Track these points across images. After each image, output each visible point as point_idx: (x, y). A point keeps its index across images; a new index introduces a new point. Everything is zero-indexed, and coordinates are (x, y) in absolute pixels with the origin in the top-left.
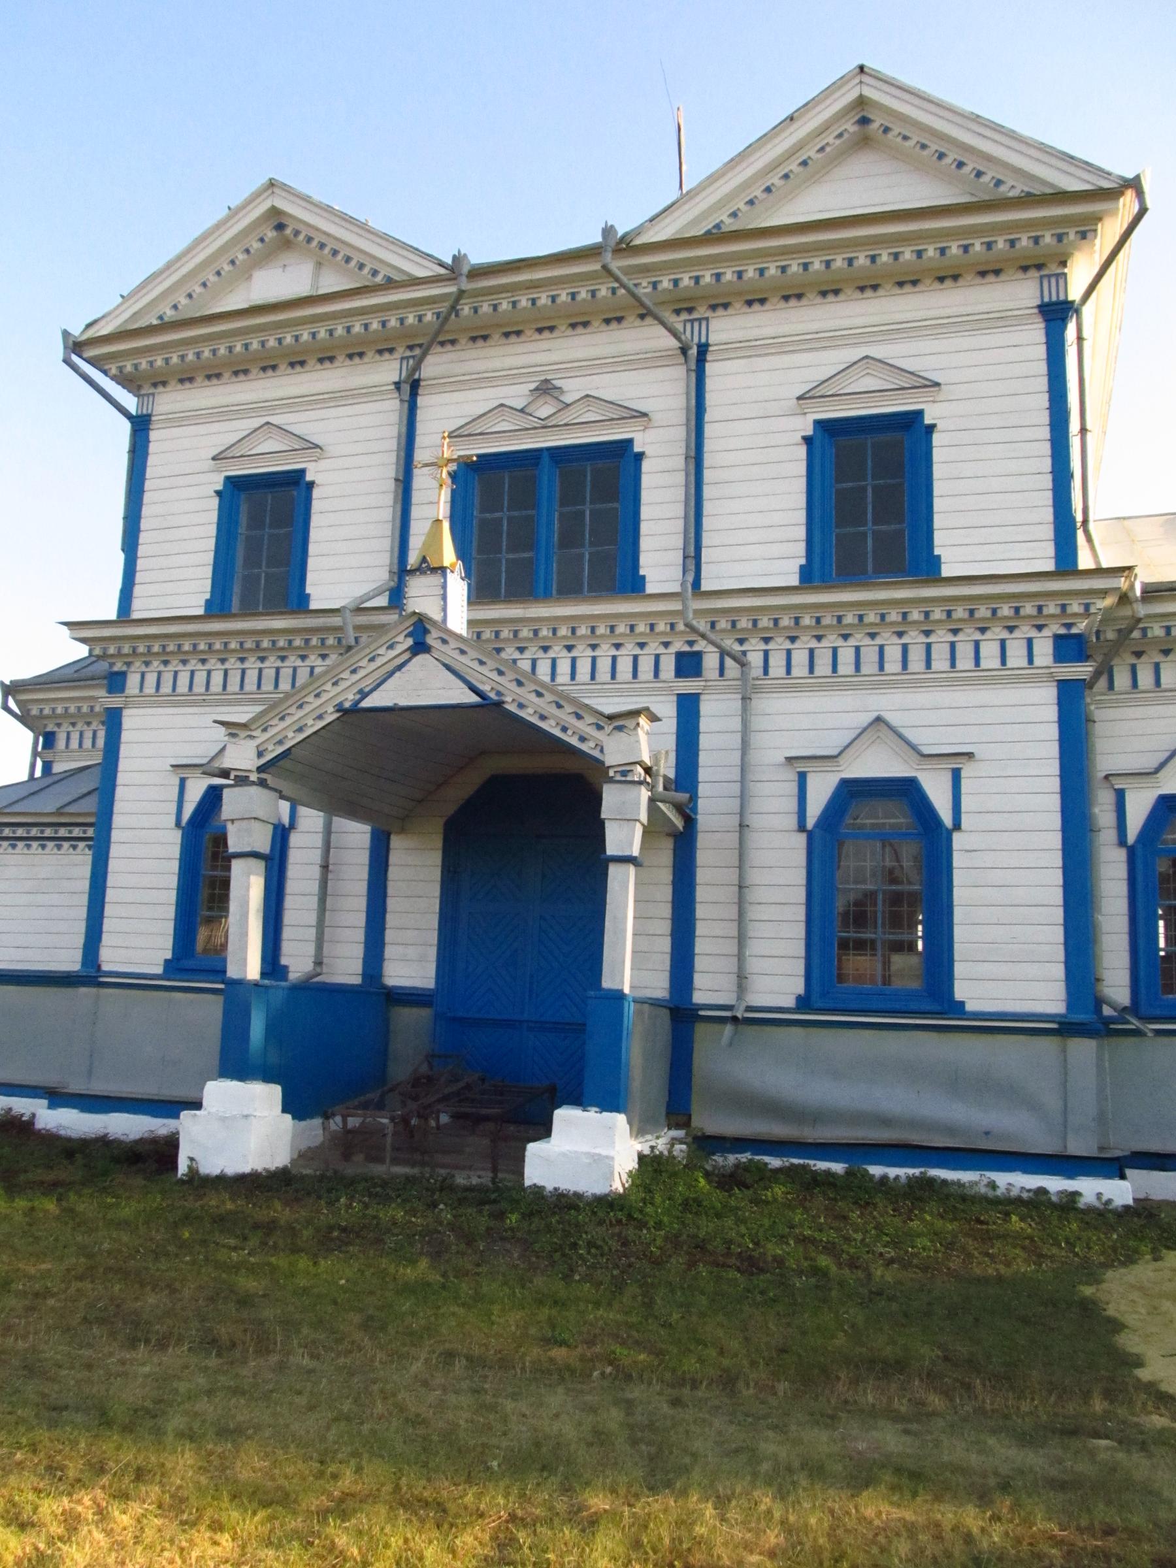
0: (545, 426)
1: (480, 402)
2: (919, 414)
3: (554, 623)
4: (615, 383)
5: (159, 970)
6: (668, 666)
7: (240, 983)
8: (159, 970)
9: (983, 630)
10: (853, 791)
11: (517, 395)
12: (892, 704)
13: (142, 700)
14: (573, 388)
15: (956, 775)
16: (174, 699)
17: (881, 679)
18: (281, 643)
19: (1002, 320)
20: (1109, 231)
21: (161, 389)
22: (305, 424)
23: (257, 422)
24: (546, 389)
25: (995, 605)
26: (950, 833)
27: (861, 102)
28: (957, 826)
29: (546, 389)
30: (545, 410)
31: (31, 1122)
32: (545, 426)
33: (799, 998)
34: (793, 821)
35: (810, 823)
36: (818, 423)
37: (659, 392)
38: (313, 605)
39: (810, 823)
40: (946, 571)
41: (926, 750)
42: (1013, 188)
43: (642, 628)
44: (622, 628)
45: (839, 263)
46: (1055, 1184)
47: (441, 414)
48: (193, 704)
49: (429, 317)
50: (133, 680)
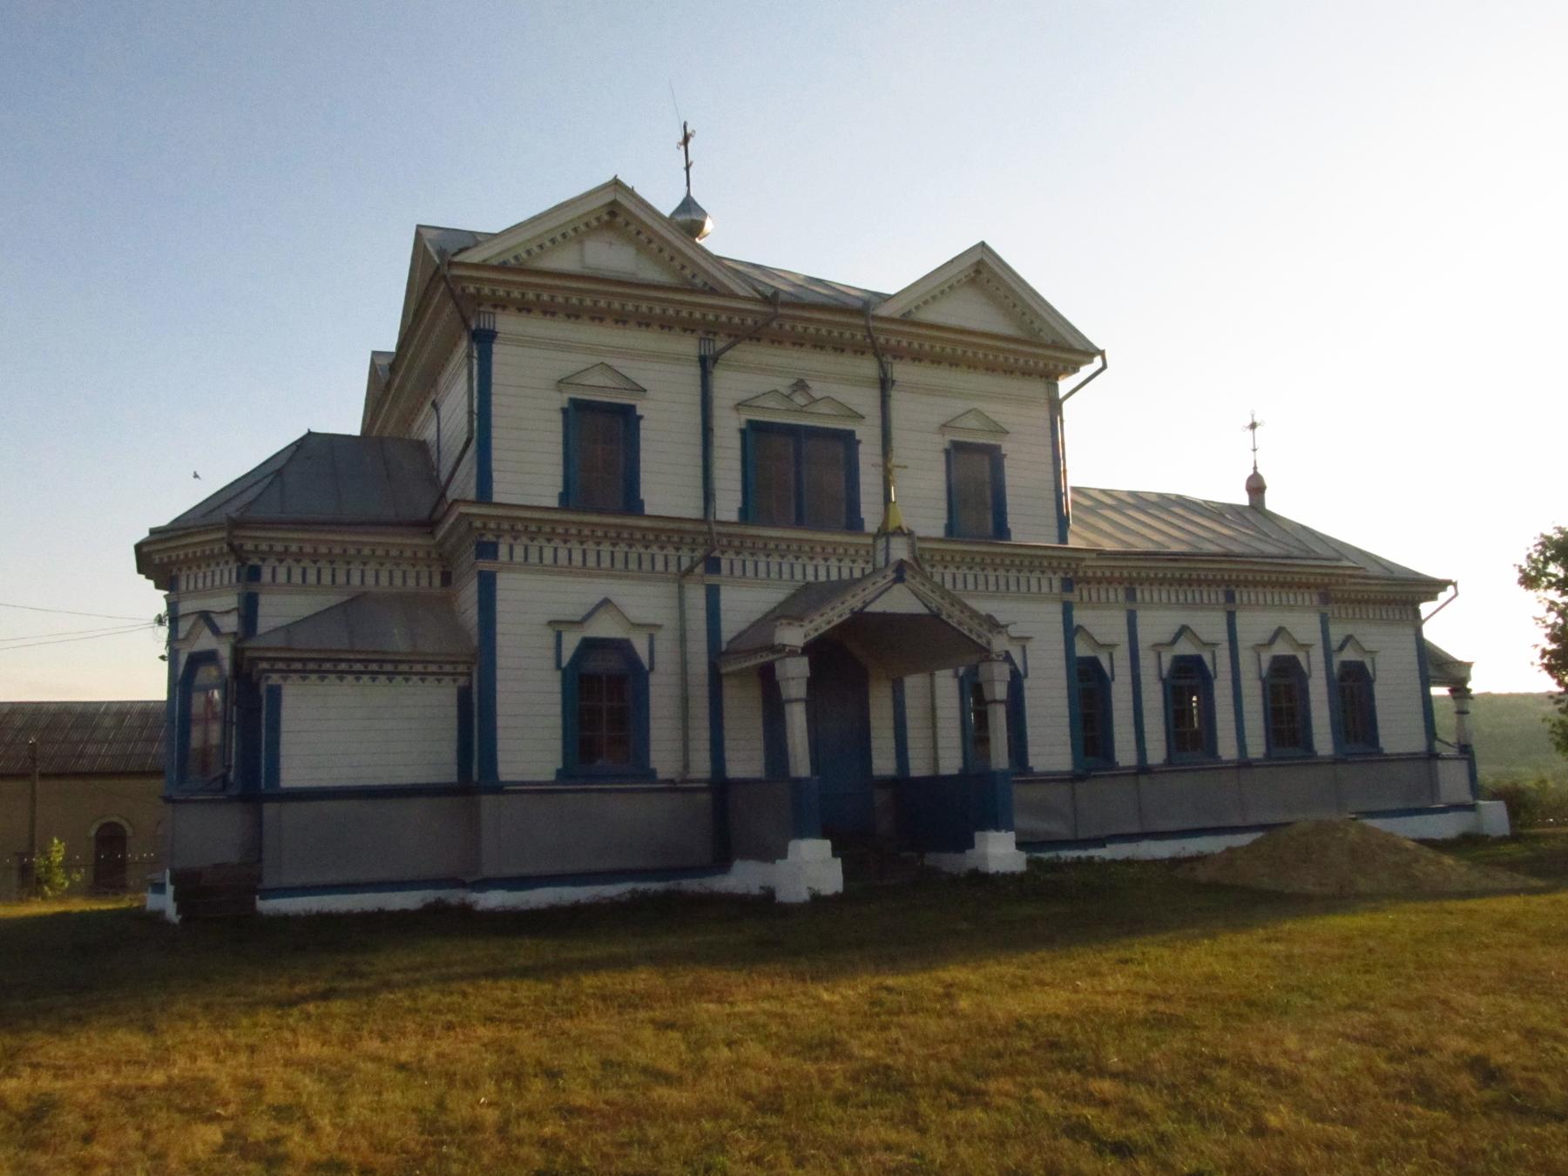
0: (801, 410)
1: (753, 382)
2: (633, 407)
3: (836, 545)
4: (839, 390)
5: (552, 778)
6: (1056, 584)
7: (798, 780)
8: (552, 778)
9: (532, 539)
10: (590, 646)
11: (783, 384)
12: (618, 590)
13: (511, 565)
14: (818, 389)
15: (1024, 648)
16: (541, 568)
17: (612, 573)
18: (599, 533)
19: (677, 359)
20: (1086, 371)
21: (499, 311)
22: (636, 371)
23: (595, 360)
24: (801, 386)
25: (671, 532)
26: (648, 673)
27: (614, 203)
28: (652, 669)
29: (801, 386)
30: (800, 399)
31: (769, 895)
32: (801, 410)
33: (559, 772)
34: (552, 664)
35: (564, 664)
36: (572, 400)
37: (865, 400)
38: (496, 498)
39: (564, 664)
40: (648, 510)
41: (579, 618)
42: (1047, 337)
43: (841, 550)
44: (830, 550)
45: (1001, 358)
46: (1083, 854)
47: (730, 385)
48: (614, 577)
49: (749, 321)
50: (503, 550)
